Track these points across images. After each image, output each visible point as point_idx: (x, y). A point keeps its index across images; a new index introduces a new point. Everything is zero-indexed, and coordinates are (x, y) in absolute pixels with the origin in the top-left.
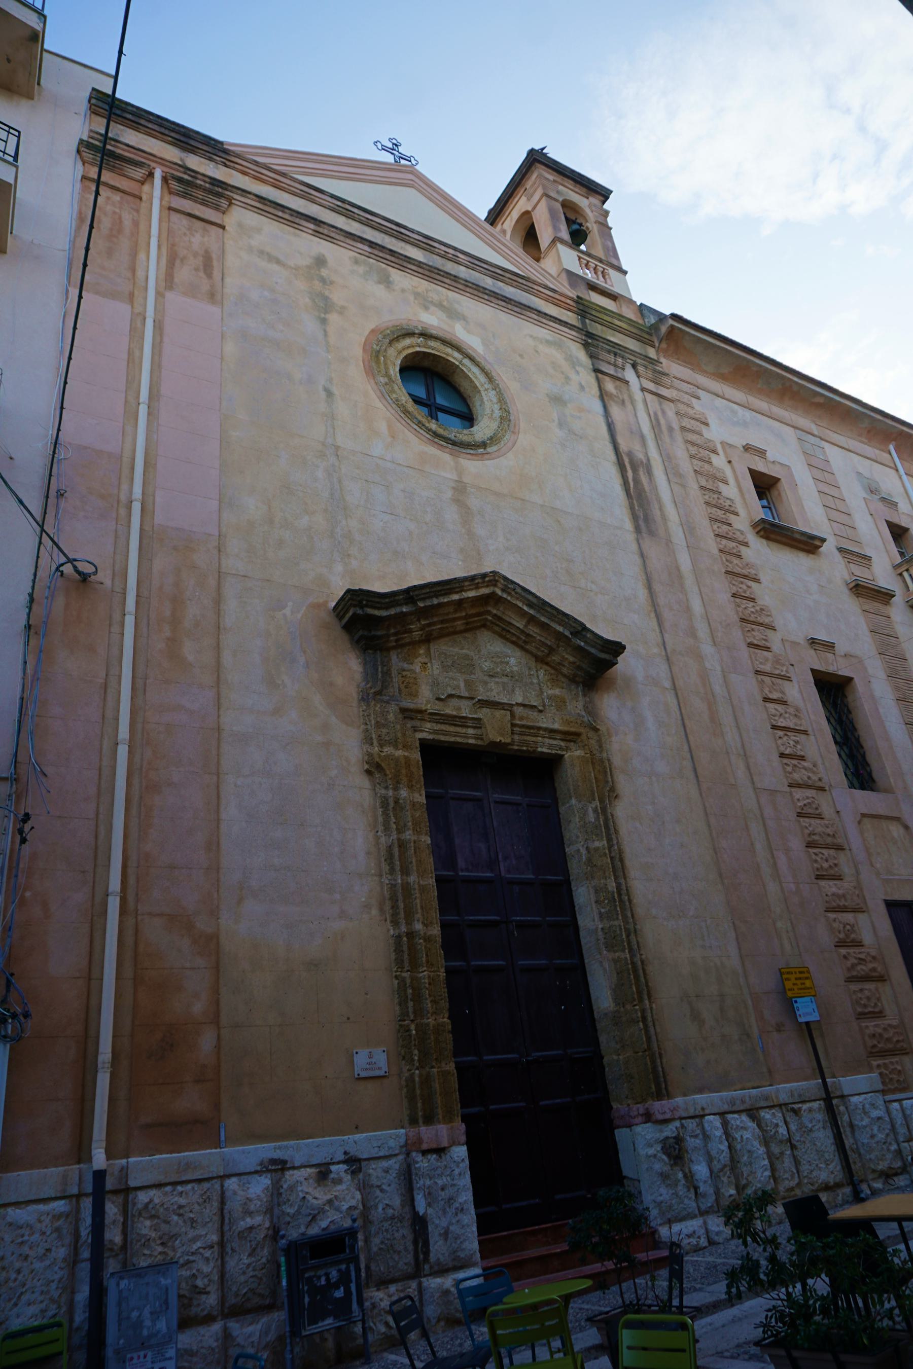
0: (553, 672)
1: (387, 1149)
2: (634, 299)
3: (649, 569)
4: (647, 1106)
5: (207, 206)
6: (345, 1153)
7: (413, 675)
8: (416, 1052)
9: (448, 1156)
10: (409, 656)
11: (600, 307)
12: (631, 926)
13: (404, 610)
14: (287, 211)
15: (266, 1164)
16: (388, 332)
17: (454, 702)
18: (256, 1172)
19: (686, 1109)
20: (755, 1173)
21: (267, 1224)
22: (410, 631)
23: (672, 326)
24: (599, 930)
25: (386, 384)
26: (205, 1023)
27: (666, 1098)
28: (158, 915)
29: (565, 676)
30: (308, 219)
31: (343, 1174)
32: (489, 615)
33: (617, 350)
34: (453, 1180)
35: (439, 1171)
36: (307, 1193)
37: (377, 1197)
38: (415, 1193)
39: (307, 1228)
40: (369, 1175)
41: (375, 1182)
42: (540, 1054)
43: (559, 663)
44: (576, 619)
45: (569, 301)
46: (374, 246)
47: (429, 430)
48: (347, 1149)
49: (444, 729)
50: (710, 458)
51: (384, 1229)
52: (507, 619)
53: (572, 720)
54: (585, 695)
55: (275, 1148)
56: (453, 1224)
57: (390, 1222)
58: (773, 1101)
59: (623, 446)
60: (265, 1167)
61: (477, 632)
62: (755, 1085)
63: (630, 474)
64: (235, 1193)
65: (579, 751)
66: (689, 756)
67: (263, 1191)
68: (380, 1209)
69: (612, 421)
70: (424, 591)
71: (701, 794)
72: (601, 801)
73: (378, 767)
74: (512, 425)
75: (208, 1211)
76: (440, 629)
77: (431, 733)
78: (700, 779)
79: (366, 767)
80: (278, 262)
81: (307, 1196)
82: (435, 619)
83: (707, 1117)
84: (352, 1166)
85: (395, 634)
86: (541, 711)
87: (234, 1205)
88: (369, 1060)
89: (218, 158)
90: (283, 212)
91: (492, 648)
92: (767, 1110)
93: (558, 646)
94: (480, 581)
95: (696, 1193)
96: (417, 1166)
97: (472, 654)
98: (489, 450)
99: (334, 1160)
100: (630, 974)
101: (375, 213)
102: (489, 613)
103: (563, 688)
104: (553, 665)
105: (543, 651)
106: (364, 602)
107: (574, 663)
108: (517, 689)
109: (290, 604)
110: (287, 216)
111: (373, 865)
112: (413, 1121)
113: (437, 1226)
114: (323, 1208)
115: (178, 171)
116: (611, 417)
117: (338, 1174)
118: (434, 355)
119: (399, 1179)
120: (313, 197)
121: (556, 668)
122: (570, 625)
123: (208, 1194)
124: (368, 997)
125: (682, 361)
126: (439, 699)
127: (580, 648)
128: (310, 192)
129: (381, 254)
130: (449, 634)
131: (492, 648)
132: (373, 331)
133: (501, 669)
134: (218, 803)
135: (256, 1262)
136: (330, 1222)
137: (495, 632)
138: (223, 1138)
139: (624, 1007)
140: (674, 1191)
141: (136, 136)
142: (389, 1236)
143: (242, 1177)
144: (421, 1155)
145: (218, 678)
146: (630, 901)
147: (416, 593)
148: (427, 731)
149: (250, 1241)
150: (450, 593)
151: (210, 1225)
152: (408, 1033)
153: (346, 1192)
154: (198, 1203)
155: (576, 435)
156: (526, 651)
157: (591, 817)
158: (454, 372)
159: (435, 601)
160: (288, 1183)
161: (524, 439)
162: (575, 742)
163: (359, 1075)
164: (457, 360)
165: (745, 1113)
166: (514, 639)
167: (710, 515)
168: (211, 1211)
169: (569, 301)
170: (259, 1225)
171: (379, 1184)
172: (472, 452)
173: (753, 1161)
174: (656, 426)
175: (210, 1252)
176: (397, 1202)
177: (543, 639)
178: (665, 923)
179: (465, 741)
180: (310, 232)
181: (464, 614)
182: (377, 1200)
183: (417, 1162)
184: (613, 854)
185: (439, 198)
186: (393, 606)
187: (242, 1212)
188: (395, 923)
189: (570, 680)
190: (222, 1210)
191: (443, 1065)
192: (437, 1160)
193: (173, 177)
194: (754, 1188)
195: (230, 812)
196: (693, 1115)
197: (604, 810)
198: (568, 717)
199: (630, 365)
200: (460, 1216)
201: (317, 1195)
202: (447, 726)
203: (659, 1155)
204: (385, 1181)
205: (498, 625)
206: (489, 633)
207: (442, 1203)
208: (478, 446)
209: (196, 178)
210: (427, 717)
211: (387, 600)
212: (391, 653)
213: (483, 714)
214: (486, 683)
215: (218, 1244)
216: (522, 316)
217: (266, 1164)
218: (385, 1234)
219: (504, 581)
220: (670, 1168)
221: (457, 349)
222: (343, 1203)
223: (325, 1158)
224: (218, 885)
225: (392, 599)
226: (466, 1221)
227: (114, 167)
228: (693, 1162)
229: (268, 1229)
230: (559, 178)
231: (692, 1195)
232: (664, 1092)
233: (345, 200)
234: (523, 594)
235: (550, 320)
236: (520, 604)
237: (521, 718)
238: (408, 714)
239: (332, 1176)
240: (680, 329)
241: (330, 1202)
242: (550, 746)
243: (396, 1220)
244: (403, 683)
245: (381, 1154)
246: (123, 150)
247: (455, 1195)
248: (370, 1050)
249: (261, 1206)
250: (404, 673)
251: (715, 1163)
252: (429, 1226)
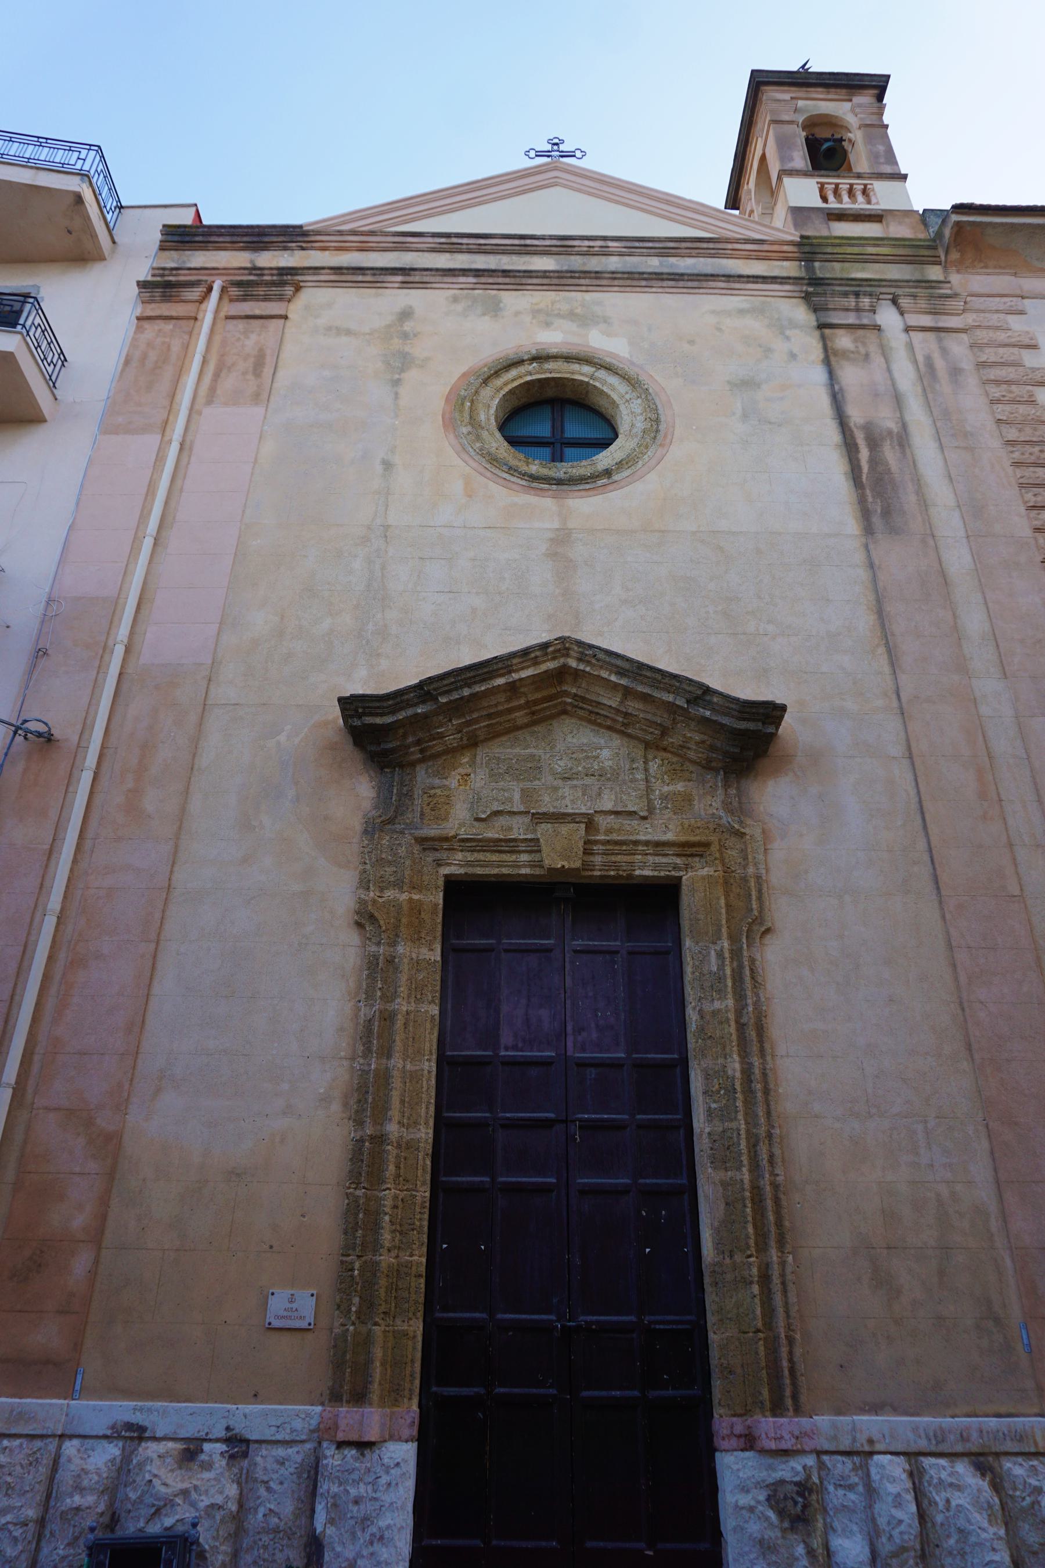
0: (675, 759)
1: (288, 1431)
2: (915, 209)
3: (880, 585)
4: (749, 1422)
5: (270, 300)
6: (228, 1429)
8: (356, 1300)
9: (375, 1456)
11: (842, 238)
12: (762, 1131)
14: (368, 272)
15: (119, 1429)
16: (486, 369)
17: (502, 821)
18: (105, 1437)
19: (835, 1438)
21: (101, 1508)
23: (958, 224)
24: (705, 1136)
25: (469, 433)
26: (83, 1241)
27: (791, 1413)
28: (55, 1109)
30: (396, 272)
31: (217, 1458)
33: (858, 288)
34: (375, 1491)
35: (355, 1476)
36: (156, 1476)
37: (259, 1497)
39: (147, 1523)
40: (255, 1464)
42: (595, 1318)
44: (691, 680)
45: (786, 248)
46: (481, 273)
47: (523, 475)
48: (231, 1423)
49: (483, 858)
50: (1031, 396)
51: (260, 1543)
54: (726, 786)
55: (135, 1409)
56: (363, 1556)
57: (271, 1536)
58: (1036, 1444)
59: (856, 415)
60: (117, 1432)
61: (555, 723)
62: (1003, 1410)
63: (864, 454)
64: (69, 1460)
65: (706, 869)
66: (926, 857)
67: (106, 1463)
68: (260, 1516)
69: (841, 389)
70: (445, 682)
71: (943, 917)
72: (733, 938)
73: (372, 917)
75: (31, 1477)
76: (488, 726)
78: (943, 893)
80: (349, 332)
82: (475, 715)
83: (876, 1457)
84: (233, 1448)
85: (418, 742)
86: (644, 818)
87: (66, 1477)
88: (290, 1306)
89: (294, 245)
90: (364, 274)
91: (575, 740)
92: (1020, 1460)
94: (538, 653)
96: (325, 1462)
97: (541, 752)
98: (615, 477)
99: (210, 1436)
100: (745, 1206)
101: (491, 235)
102: (566, 694)
103: (689, 781)
106: (360, 710)
107: (703, 742)
108: (607, 791)
110: (369, 278)
111: (344, 1045)
112: (335, 1397)
113: (338, 1555)
114: (172, 1500)
115: (243, 275)
116: (838, 383)
117: (211, 1456)
118: (553, 378)
119: (299, 1477)
120: (408, 245)
122: (685, 690)
123: (38, 1455)
124: (305, 1219)
125: (995, 267)
128: (405, 241)
129: (491, 280)
130: (508, 731)
131: (575, 740)
132: (464, 375)
133: (584, 767)
134: (152, 975)
135: (74, 1555)
136: (178, 1521)
137: (581, 718)
138: (78, 1387)
139: (731, 1257)
141: (205, 255)
142: (266, 1556)
143: (87, 1441)
144: (334, 1447)
146: (766, 1091)
147: (435, 685)
148: (456, 865)
149: (75, 1526)
151: (29, 1495)
152: (350, 1273)
153: (213, 1483)
154: (22, 1466)
155: (770, 423)
156: (629, 736)
157: (714, 965)
158: (587, 392)
159: (466, 692)
160: (138, 1458)
161: (676, 452)
162: (701, 856)
163: (270, 1324)
164: (587, 376)
165: (966, 1459)
166: (609, 723)
167: (1021, 481)
168: (34, 1477)
169: (786, 248)
170: (89, 1508)
171: (266, 1478)
172: (588, 486)
173: (968, 1549)
174: (927, 374)
175: (21, 1531)
176: (288, 1508)
177: (649, 717)
179: (515, 871)
180: (397, 285)
181: (522, 701)
183: (326, 1457)
184: (744, 1020)
185: (592, 184)
186: (402, 709)
187: (72, 1486)
188: (359, 1123)
189: (704, 767)
190: (52, 1479)
191: (398, 1322)
192: (356, 1459)
193: (232, 284)
195: (166, 985)
196: (848, 1449)
198: (693, 821)
199: (889, 302)
200: (377, 1547)
201: (169, 1481)
202: (488, 854)
203: (760, 1508)
204: (275, 1476)
205: (582, 708)
206: (573, 721)
207: (352, 1522)
209: (263, 275)
210: (456, 845)
211: (390, 703)
212: (418, 768)
213: (544, 830)
214: (556, 789)
215: (37, 1522)
216: (701, 291)
217: (119, 1429)
218: (262, 1551)
219: (579, 647)
220: (779, 1534)
221: (587, 361)
222: (203, 1498)
223: (199, 1432)
224: (133, 1074)
225: (398, 700)
226: (385, 1556)
227: (171, 296)
228: (834, 1531)
229: (102, 1514)
230: (795, 92)
232: (789, 1402)
233: (451, 234)
234: (608, 659)
235: (748, 282)
236: (604, 674)
237: (609, 831)
238: (427, 844)
239: (203, 1457)
240: (974, 223)
241: (185, 1493)
242: (656, 867)
243: (281, 1535)
244: (429, 804)
245: (279, 1437)
246: (185, 275)
247: (374, 1515)
248: (292, 1292)
249: (97, 1483)
250: (432, 792)
251: (884, 1539)
252: (326, 1554)
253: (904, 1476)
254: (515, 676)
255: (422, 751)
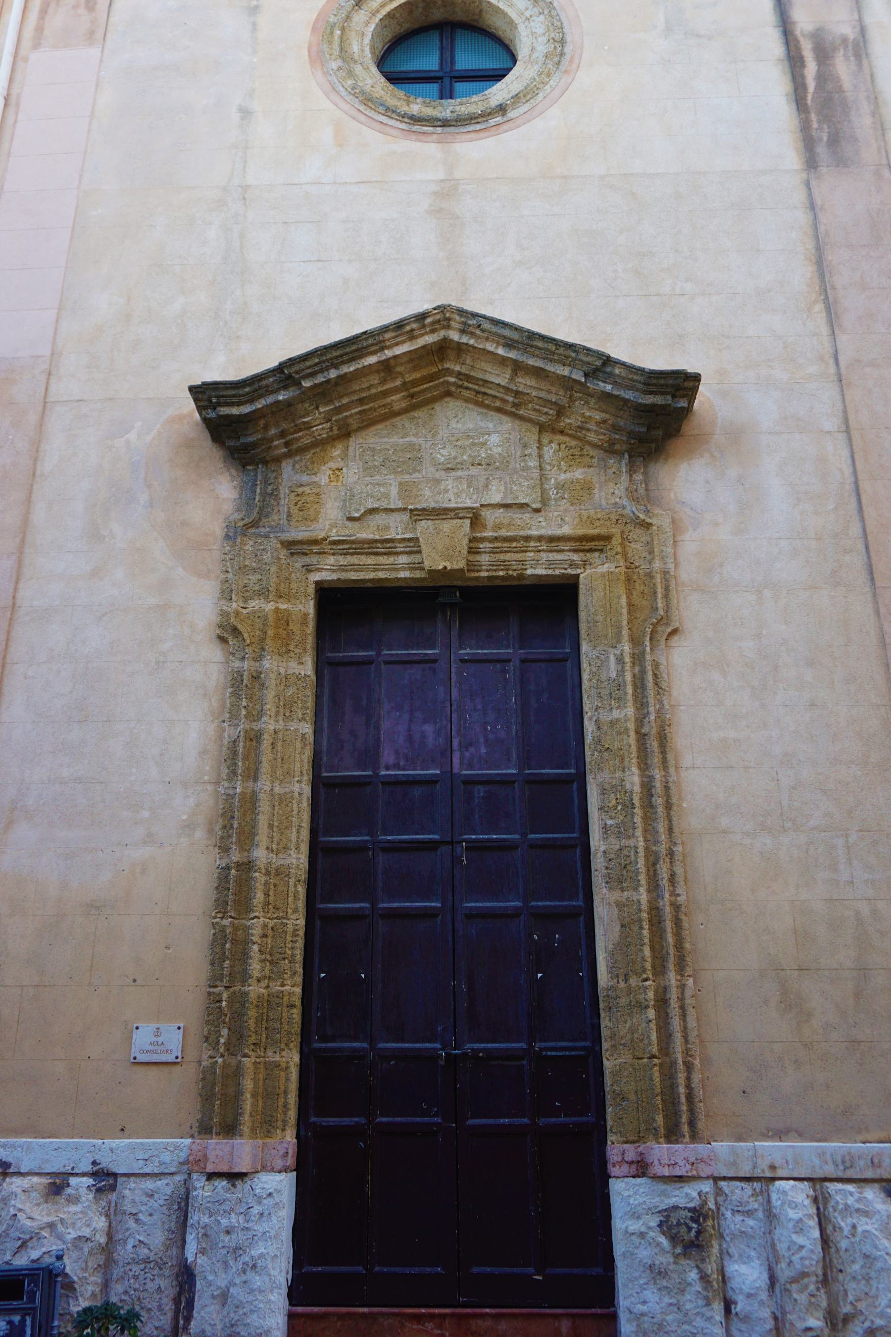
0: (573, 443)
6: (94, 1163)
7: (315, 490)
8: (225, 1032)
9: (247, 1186)
10: (313, 463)
12: (662, 849)
13: (281, 398)
17: (379, 519)
20: (877, 1297)
22: (308, 426)
29: (595, 446)
31: (83, 1191)
32: (450, 375)
35: (226, 1206)
36: (20, 1210)
37: (128, 1229)
38: (189, 1229)
41: (128, 1207)
43: (579, 427)
44: (588, 349)
48: (98, 1158)
49: (356, 562)
51: (131, 1274)
52: (480, 375)
53: (599, 516)
54: (631, 471)
56: (235, 1284)
57: (142, 1266)
63: (811, 69)
65: (606, 565)
66: (860, 546)
70: (308, 363)
71: (877, 612)
72: (635, 641)
73: (235, 630)
74: (565, 61)
76: (360, 412)
77: (334, 571)
79: (218, 631)
81: (19, 1214)
82: (345, 401)
83: (777, 1183)
86: (537, 511)
91: (460, 426)
93: (572, 399)
94: (414, 326)
95: (728, 1310)
97: (421, 441)
98: (511, 114)
99: (76, 1171)
102: (449, 372)
104: (570, 432)
105: (546, 413)
106: (214, 400)
107: (605, 422)
108: (494, 482)
109: (138, 424)
111: (207, 768)
112: (205, 1129)
121: (578, 433)
124: (170, 951)
126: (351, 519)
127: (606, 397)
130: (383, 418)
131: (460, 426)
133: (470, 456)
137: (467, 400)
139: (626, 981)
140: (673, 1301)
142: (137, 1286)
144: (204, 1178)
145: (23, 541)
147: (296, 368)
150: (361, 357)
152: (218, 1004)
153: (80, 1216)
155: (698, 36)
156: (522, 418)
159: (333, 374)
162: (601, 551)
163: (135, 1058)
165: (876, 1185)
166: (498, 404)
171: (134, 1211)
172: (478, 127)
177: (543, 395)
178: (747, 841)
179: (393, 575)
181: (398, 382)
182: (127, 1234)
186: (261, 396)
188: (225, 850)
189: (606, 451)
191: (270, 1053)
192: (227, 1190)
194: (867, 1324)
197: (638, 658)
198: (592, 512)
200: (250, 1275)
202: (363, 557)
204: (143, 1208)
205: (467, 388)
206: (459, 403)
207: (224, 1251)
208: (490, 114)
210: (327, 548)
211: (247, 390)
212: (284, 464)
214: (438, 481)
218: (132, 1281)
219: (461, 316)
220: (672, 1260)
222: (70, 1230)
225: (256, 386)
231: (717, 1310)
232: (685, 1129)
234: (494, 329)
236: (490, 347)
237: (498, 527)
239: (69, 1191)
241: (51, 1226)
242: (550, 564)
243: (152, 1265)
244: (296, 504)
245: (147, 1170)
250: (300, 490)
251: (783, 1265)
252: (198, 1283)
253: (807, 1202)
254: (389, 353)
255: (287, 444)
